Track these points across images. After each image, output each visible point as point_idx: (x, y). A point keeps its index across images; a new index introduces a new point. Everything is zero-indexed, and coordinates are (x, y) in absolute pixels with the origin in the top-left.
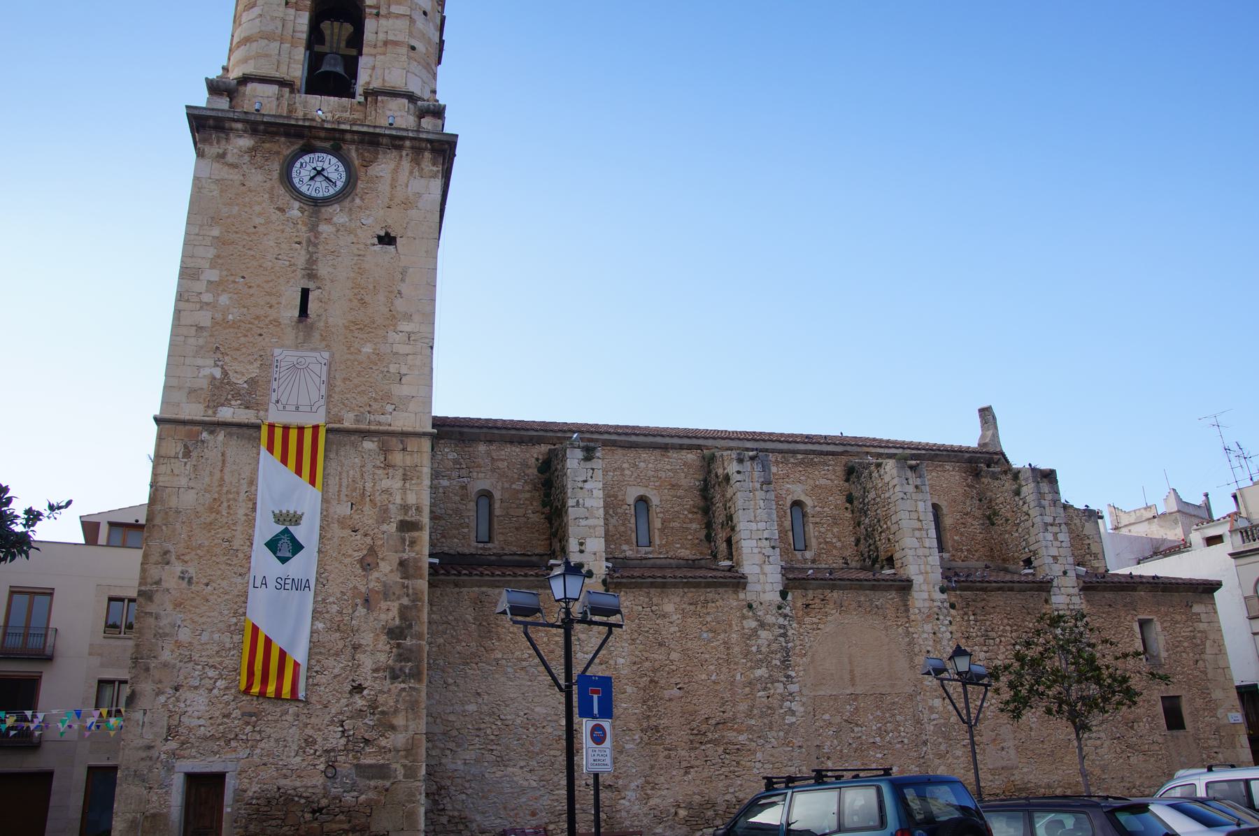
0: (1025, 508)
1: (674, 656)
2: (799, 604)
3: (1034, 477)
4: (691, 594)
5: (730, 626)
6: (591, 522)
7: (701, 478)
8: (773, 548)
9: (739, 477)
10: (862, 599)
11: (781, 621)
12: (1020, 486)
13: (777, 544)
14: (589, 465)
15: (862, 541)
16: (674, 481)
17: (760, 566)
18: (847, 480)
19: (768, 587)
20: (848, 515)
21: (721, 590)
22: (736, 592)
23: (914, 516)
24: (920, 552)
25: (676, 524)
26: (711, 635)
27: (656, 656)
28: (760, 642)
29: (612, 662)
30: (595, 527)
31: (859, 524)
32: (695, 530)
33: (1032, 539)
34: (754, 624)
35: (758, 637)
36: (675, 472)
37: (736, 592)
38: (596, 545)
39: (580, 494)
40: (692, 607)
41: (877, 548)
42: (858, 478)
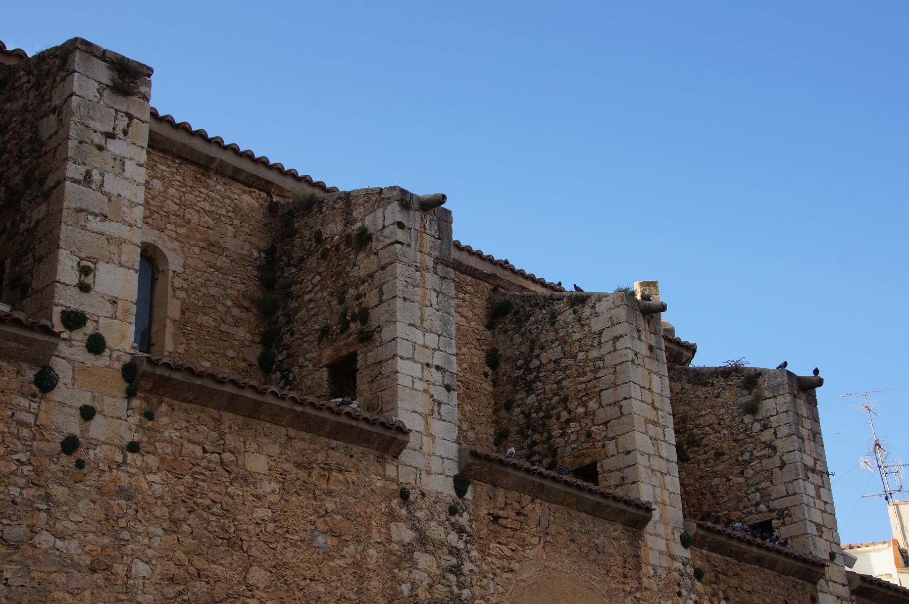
0: (767, 435)
1: (258, 576)
2: (483, 512)
3: (791, 386)
4: (302, 443)
5: (368, 530)
6: (110, 228)
7: (263, 245)
8: (448, 388)
9: (400, 235)
10: (576, 527)
11: (453, 537)
12: (760, 398)
13: (455, 383)
14: (122, 104)
15: (513, 436)
16: (213, 235)
17: (425, 418)
18: (490, 326)
19: (436, 464)
20: (487, 386)
21: (356, 449)
22: (381, 460)
23: (647, 397)
24: (657, 463)
25: (208, 321)
26: (331, 542)
27: (219, 570)
28: (416, 575)
29: (119, 569)
30: (121, 242)
31: (508, 406)
32: (243, 345)
33: (778, 489)
34: (408, 535)
35: (415, 566)
36: (217, 218)
37: (381, 460)
38: (119, 282)
39: (96, 160)
40: (302, 474)
41: (553, 451)
42: (519, 323)
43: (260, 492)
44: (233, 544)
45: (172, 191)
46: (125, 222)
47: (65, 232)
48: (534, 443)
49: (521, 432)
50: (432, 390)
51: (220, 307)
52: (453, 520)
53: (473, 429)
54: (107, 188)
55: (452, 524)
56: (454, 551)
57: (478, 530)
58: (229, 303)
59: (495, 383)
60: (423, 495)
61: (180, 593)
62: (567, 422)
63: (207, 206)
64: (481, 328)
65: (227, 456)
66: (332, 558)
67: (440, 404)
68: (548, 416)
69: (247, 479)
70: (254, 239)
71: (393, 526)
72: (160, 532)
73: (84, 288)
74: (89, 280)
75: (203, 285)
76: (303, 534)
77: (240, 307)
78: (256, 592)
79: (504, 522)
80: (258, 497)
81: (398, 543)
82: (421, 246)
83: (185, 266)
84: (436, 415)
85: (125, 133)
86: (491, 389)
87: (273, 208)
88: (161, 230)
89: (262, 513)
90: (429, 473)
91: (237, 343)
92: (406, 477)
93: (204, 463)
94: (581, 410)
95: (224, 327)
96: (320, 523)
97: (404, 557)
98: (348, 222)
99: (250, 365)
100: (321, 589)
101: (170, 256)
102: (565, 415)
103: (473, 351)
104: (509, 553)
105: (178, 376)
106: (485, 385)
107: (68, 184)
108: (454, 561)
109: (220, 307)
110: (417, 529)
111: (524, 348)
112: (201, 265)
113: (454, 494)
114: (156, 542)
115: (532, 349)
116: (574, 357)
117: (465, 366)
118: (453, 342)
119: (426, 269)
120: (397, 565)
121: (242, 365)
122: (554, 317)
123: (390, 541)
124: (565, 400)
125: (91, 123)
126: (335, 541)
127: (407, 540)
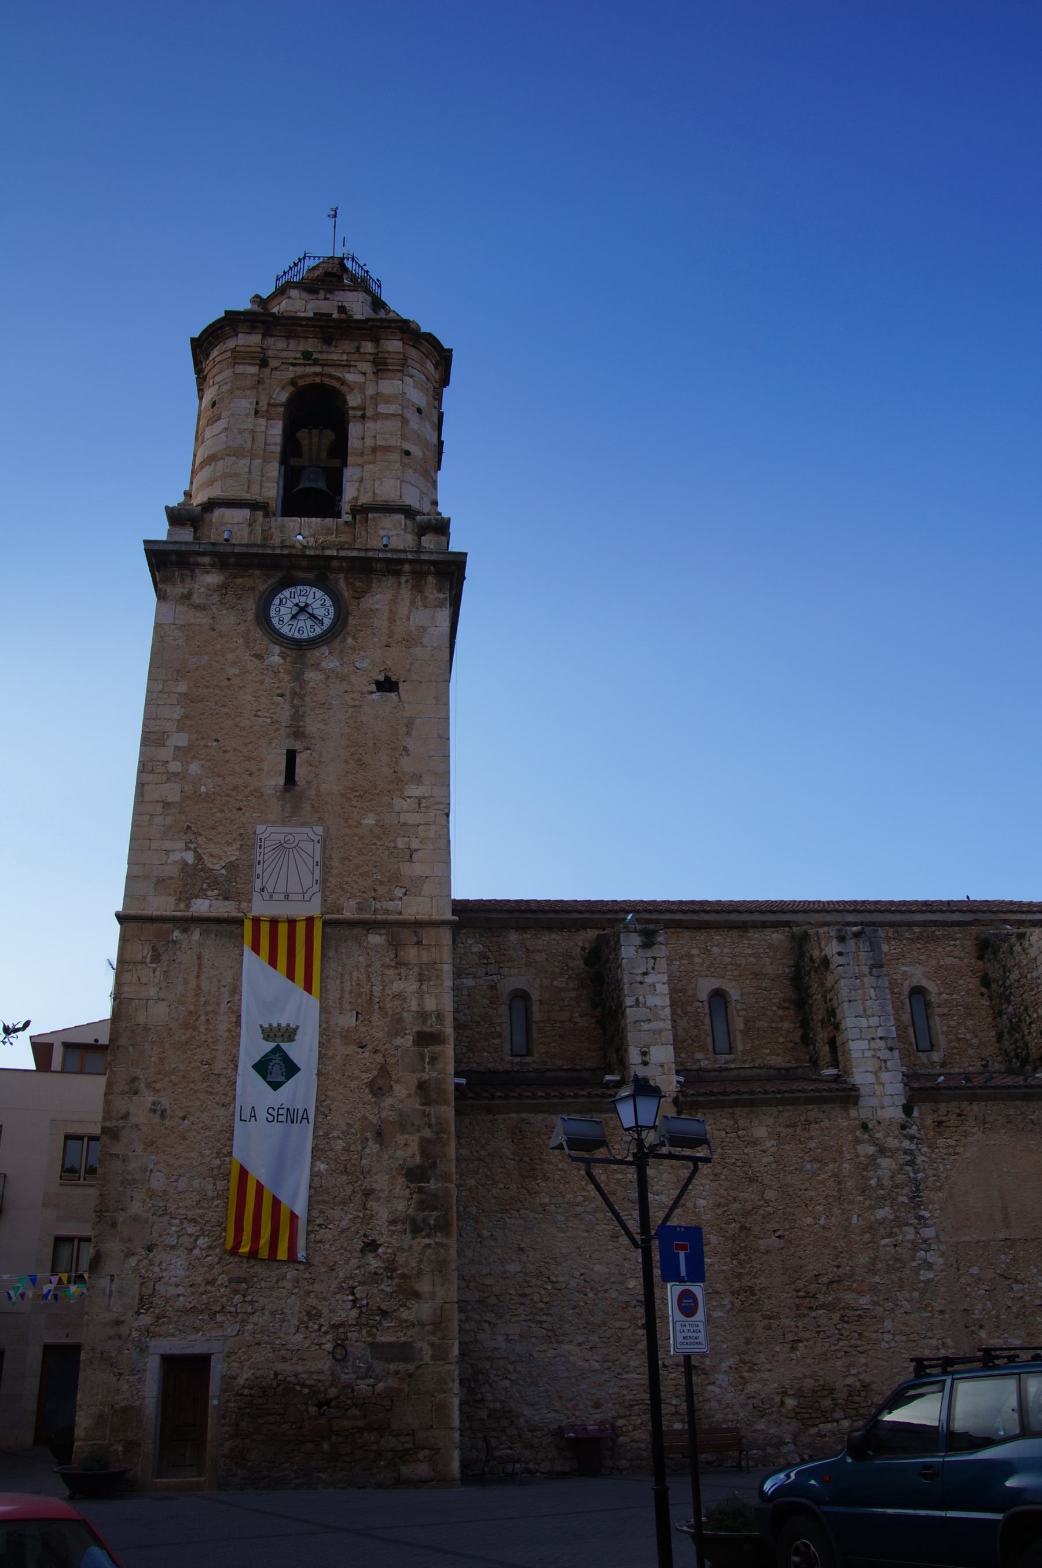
1: (770, 1194)
2: (929, 1122)
5: (841, 1153)
7: (792, 962)
8: (891, 1049)
11: (906, 1144)
14: (649, 953)
15: (1006, 1036)
17: (875, 1073)
18: (980, 957)
19: (887, 1101)
20: (985, 1002)
34: (871, 1150)
35: (878, 1167)
40: (790, 1131)
43: (765, 1148)
44: (752, 1180)
45: (726, 950)
46: (661, 1019)
47: (630, 1036)
48: (1017, 1041)
49: (1009, 1033)
50: (879, 1054)
51: (769, 1013)
52: (905, 1132)
53: (977, 1036)
54: (648, 1004)
55: (904, 1136)
56: (906, 1152)
57: (926, 1134)
58: (775, 1008)
59: (990, 998)
60: (879, 1123)
61: (725, 1212)
62: (1030, 1024)
63: (749, 951)
64: (973, 961)
65: (740, 1133)
66: (819, 1175)
67: (885, 1061)
68: (1020, 1021)
69: (754, 1143)
70: (784, 961)
71: (859, 1147)
72: (708, 1182)
73: (645, 1063)
74: (646, 1059)
75: (756, 1002)
76: (796, 1166)
77: (782, 1008)
78: (771, 1204)
79: (947, 1124)
80: (764, 1151)
81: (864, 1156)
82: (858, 961)
83: (742, 995)
84: (883, 1069)
85: (653, 968)
86: (988, 1003)
87: (793, 937)
88: (723, 977)
89: (766, 1160)
90: (882, 1108)
91: (306, 1391)
92: (864, 1114)
93: (728, 1140)
94: (1035, 1015)
95: (774, 1025)
96: (806, 1158)
97: (872, 1162)
98: (821, 951)
99: (796, 1043)
100: (812, 1194)
101: (732, 992)
102: (1028, 1020)
103: (969, 980)
104: (954, 1143)
105: (701, 1099)
106: (982, 1002)
107: (628, 1010)
108: (908, 1158)
109: (769, 1013)
110: (877, 1145)
111: (1001, 972)
112: (752, 990)
113: (903, 1116)
114: (707, 1187)
115: (1005, 973)
116: (1026, 977)
117: (963, 993)
118: (891, 1017)
119: (865, 975)
120: (865, 1170)
121: (791, 1045)
122: (1011, 948)
123: (858, 1156)
124: (1026, 1009)
125: (635, 971)
126: (819, 1165)
127: (870, 1153)
